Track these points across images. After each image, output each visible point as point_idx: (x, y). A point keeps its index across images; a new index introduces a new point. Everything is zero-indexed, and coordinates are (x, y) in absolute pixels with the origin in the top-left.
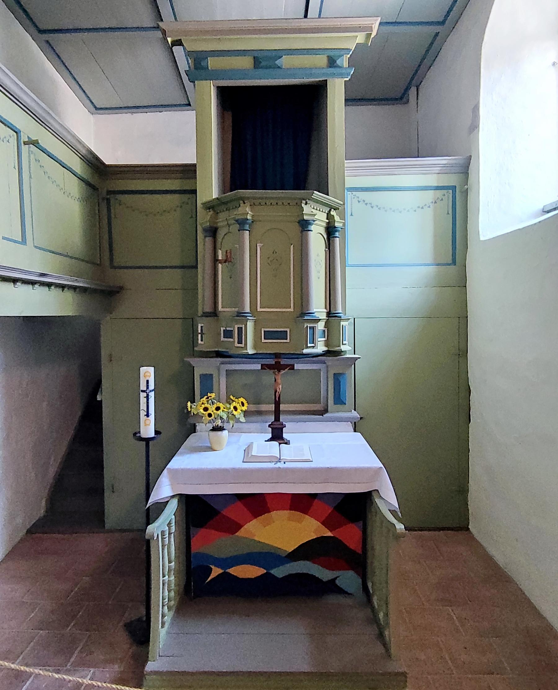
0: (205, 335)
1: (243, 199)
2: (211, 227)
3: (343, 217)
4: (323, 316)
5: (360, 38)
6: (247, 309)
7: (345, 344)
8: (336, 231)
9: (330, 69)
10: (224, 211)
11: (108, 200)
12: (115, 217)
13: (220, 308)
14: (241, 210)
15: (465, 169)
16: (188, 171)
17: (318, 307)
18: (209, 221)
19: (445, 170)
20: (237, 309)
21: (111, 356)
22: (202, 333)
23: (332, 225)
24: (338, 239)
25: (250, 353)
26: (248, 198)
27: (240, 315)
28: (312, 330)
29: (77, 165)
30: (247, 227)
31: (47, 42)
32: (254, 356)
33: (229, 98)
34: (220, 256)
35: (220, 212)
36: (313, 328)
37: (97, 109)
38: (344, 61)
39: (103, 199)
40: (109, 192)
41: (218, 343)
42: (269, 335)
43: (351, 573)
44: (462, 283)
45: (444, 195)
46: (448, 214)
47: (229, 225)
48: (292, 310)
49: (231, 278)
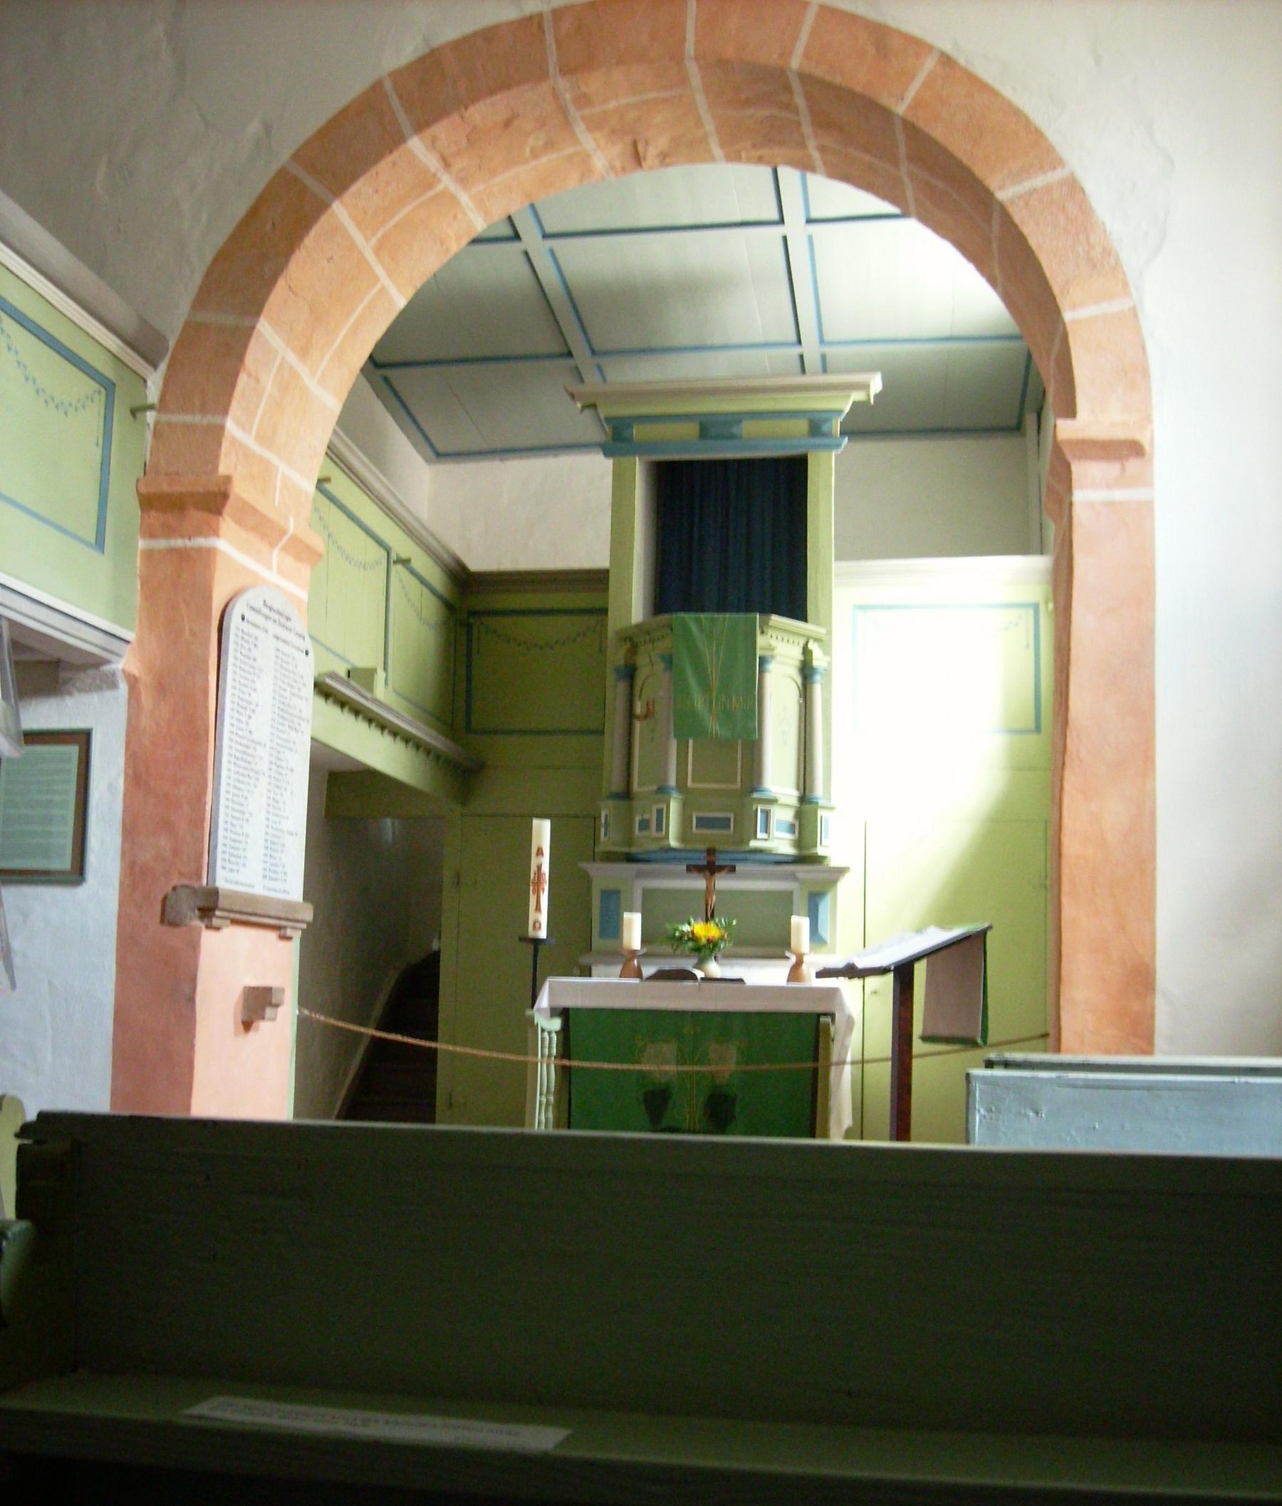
3: (827, 651)
5: (858, 396)
6: (672, 781)
12: (478, 652)
13: (635, 787)
16: (596, 580)
17: (778, 776)
21: (458, 875)
27: (662, 790)
29: (435, 576)
31: (386, 379)
34: (639, 709)
36: (767, 814)
37: (440, 455)
42: (702, 822)
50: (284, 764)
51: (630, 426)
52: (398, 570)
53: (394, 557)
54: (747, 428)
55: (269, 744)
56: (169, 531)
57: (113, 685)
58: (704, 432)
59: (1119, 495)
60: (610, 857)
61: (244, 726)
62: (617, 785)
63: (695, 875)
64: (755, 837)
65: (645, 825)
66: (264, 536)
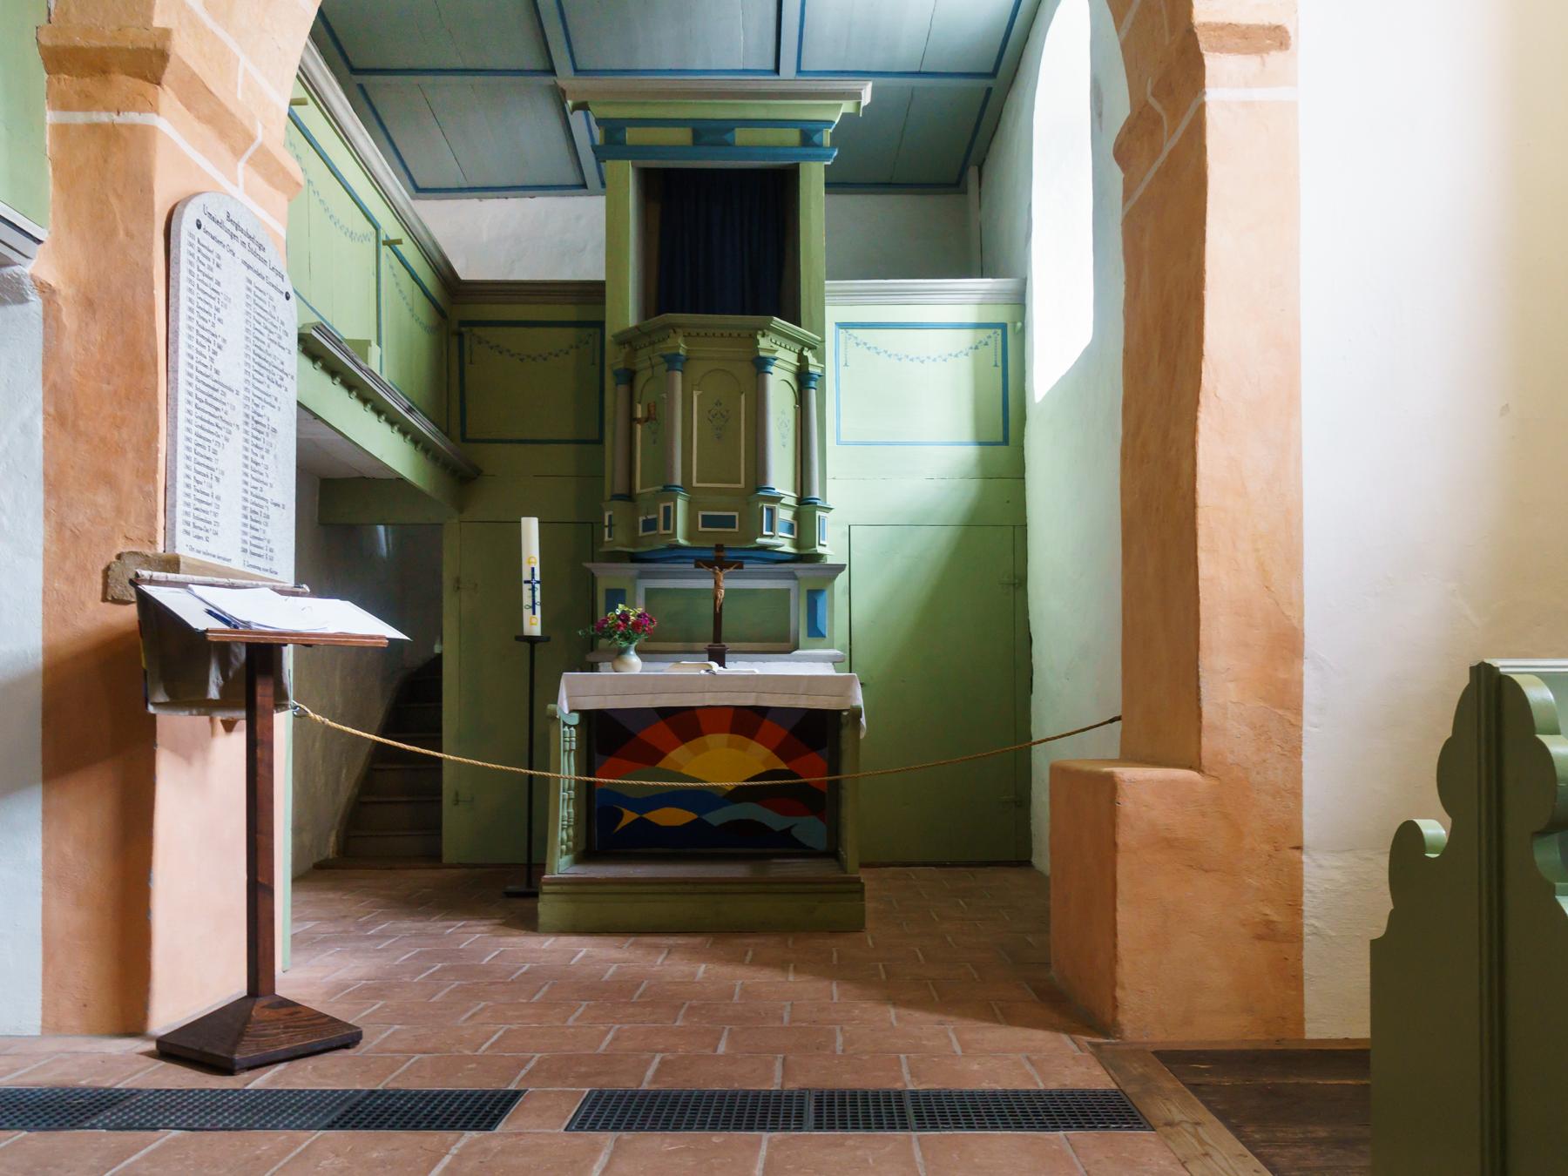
1: (674, 327)
2: (626, 369)
3: (821, 359)
5: (847, 107)
6: (678, 482)
11: (461, 335)
13: (638, 489)
15: (1020, 301)
16: (591, 293)
17: (780, 478)
21: (458, 580)
26: (680, 326)
27: (669, 490)
30: (679, 365)
31: (361, 86)
34: (639, 412)
36: (771, 511)
38: (826, 137)
40: (463, 323)
41: (636, 541)
43: (812, 819)
48: (742, 485)
50: (264, 421)
51: (622, 129)
52: (385, 250)
53: (383, 238)
54: (741, 136)
55: (242, 392)
56: (88, 101)
57: (22, 299)
58: (697, 136)
59: (1257, 94)
60: (616, 557)
61: (206, 362)
62: (620, 488)
63: (705, 570)
65: (650, 525)
66: (223, 135)
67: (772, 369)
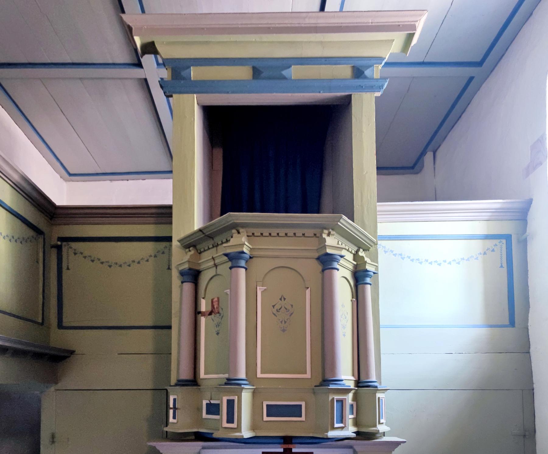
0: (179, 411)
1: (236, 227)
2: (190, 269)
3: (375, 259)
4: (352, 385)
6: (242, 375)
7: (383, 423)
8: (368, 276)
9: (356, 80)
10: (209, 249)
11: (59, 248)
13: (202, 374)
14: (233, 242)
15: (522, 215)
17: (346, 374)
18: (189, 261)
19: (498, 215)
20: (226, 376)
21: (53, 436)
22: (175, 408)
23: (361, 268)
24: (369, 286)
25: (245, 437)
28: (340, 404)
30: (243, 263)
32: (250, 441)
33: (221, 123)
34: (204, 306)
35: (205, 251)
36: (341, 402)
39: (53, 247)
41: (200, 421)
42: (273, 411)
44: (524, 349)
45: (496, 245)
46: (502, 266)
47: (216, 266)
48: (308, 375)
49: (218, 334)
54: (295, 72)
58: (257, 73)
62: (186, 374)
64: (333, 428)
67: (336, 265)
